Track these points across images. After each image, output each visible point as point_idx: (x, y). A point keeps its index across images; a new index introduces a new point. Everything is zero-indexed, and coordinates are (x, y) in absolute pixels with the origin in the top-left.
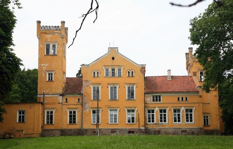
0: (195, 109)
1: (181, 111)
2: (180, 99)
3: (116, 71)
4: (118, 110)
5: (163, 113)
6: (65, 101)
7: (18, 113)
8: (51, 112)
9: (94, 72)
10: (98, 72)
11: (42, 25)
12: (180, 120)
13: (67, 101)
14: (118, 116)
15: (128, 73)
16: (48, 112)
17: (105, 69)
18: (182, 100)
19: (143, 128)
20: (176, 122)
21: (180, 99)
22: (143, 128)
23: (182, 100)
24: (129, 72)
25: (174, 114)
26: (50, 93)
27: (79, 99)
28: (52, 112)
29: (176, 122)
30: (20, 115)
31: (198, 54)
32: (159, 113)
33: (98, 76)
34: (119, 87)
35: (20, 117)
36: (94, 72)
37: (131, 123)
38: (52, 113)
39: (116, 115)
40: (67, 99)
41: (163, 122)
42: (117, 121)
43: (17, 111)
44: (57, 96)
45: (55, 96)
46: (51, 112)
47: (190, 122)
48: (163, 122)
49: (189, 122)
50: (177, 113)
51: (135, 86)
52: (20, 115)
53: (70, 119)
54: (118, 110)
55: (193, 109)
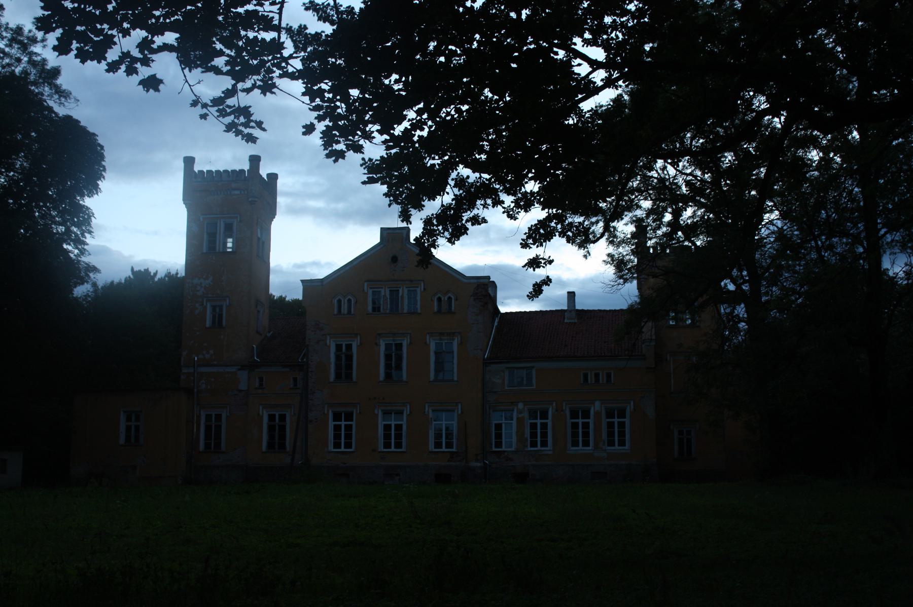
0: (632, 407)
1: (592, 412)
2: (591, 378)
3: (219, 241)
4: (407, 411)
5: (616, 420)
6: (257, 384)
7: (123, 418)
8: (216, 415)
9: (339, 301)
10: (349, 300)
11: (196, 168)
12: (589, 441)
13: (261, 385)
14: (404, 427)
15: (436, 303)
16: (208, 417)
17: (370, 292)
18: (597, 380)
19: (479, 464)
20: (578, 446)
21: (591, 378)
22: (479, 464)
23: (597, 380)
24: (439, 299)
25: (573, 423)
26: (215, 363)
27: (295, 380)
28: (219, 417)
29: (578, 446)
30: (129, 423)
31: (498, 98)
32: (604, 421)
33: (349, 312)
34: (411, 343)
35: (128, 429)
36: (339, 301)
37: (393, 449)
38: (285, 421)
39: (399, 427)
40: (261, 379)
41: (539, 447)
42: (404, 444)
43: (122, 413)
44: (233, 369)
45: (229, 369)
46: (216, 415)
47: (619, 445)
48: (539, 447)
49: (617, 447)
50: (343, 423)
51: (456, 340)
52: (129, 423)
53: (271, 437)
54: (407, 411)
55: (628, 408)
